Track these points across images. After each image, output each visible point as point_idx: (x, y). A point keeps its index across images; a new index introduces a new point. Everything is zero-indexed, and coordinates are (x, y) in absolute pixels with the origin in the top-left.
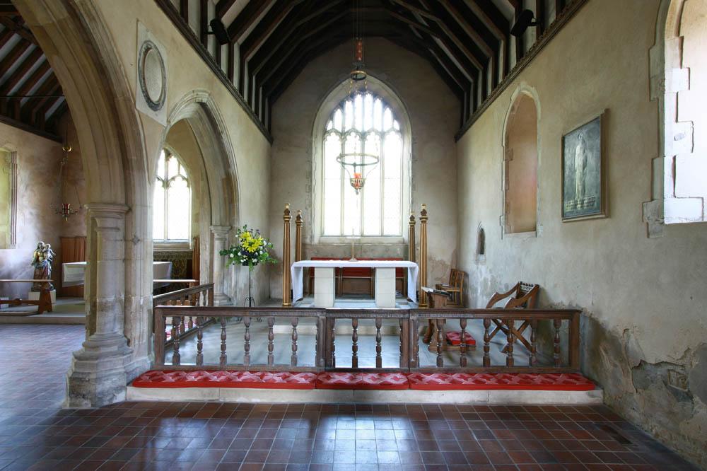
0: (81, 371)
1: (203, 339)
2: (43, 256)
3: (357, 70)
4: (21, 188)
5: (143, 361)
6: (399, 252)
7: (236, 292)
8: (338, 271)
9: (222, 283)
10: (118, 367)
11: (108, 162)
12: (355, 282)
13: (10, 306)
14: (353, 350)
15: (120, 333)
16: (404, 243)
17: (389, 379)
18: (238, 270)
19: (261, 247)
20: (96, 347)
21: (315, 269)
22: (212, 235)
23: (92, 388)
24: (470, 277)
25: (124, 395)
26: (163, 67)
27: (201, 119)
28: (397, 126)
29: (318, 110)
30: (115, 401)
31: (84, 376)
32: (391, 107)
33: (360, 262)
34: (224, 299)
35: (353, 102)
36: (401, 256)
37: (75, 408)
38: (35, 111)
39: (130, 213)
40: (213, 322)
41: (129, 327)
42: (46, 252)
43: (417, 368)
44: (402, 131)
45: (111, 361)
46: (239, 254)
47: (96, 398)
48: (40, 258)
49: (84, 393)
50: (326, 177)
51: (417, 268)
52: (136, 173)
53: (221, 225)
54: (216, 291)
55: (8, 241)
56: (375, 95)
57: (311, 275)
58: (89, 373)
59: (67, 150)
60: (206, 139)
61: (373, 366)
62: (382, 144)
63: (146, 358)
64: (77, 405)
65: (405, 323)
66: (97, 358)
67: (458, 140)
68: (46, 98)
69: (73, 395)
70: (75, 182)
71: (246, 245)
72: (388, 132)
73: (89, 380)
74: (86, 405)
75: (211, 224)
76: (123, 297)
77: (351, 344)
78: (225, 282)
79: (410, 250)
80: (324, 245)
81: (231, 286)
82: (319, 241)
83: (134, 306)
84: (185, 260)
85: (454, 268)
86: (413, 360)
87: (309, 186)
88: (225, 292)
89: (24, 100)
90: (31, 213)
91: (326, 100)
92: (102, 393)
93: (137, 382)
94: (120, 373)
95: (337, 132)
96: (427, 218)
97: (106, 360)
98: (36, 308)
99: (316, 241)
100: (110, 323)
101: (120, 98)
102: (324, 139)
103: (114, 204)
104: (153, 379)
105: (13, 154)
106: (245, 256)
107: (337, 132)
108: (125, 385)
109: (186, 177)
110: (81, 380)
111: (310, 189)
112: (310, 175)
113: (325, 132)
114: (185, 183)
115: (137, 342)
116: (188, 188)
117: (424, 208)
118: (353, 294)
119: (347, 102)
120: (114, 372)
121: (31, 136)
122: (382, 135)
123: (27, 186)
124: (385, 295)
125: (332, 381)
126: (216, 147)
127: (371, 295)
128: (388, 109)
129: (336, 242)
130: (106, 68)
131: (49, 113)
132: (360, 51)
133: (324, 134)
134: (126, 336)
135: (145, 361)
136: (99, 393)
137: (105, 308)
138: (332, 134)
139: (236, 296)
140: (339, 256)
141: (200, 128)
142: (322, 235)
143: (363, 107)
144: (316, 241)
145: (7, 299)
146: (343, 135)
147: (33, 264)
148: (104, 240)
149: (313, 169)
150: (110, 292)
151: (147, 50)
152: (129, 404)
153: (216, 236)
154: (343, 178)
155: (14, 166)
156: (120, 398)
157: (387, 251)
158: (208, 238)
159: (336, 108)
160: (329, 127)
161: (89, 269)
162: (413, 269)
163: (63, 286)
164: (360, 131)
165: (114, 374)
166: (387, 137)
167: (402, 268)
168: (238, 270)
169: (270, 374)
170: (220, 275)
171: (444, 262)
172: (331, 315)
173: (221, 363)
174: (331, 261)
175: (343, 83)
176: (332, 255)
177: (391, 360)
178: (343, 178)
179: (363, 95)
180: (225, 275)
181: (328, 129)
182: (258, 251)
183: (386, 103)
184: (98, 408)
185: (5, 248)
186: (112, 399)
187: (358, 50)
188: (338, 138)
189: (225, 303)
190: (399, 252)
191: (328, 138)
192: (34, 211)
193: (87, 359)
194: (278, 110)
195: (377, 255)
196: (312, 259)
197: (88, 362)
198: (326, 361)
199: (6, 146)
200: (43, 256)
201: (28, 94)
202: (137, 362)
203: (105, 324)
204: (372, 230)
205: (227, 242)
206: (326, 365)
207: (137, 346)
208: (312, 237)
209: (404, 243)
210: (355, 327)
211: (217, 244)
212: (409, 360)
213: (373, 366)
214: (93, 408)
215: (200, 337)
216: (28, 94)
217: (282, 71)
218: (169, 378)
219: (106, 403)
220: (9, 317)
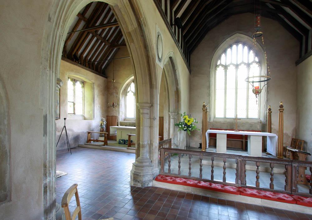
0: (137, 171)
1: (171, 163)
3: (257, 32)
4: (96, 96)
5: (156, 170)
6: (259, 127)
7: (179, 143)
8: (229, 136)
9: (174, 138)
10: (150, 172)
11: (146, 85)
12: (239, 142)
13: (94, 142)
14: (212, 172)
15: (148, 157)
16: (261, 123)
17: (227, 188)
18: (180, 133)
19: (193, 123)
20: (142, 162)
21: (217, 134)
22: (169, 116)
23: (141, 179)
24: (308, 144)
25: (152, 184)
26: (162, 43)
27: (169, 64)
28: (257, 59)
29: (213, 55)
30: (149, 186)
31: (138, 174)
32: (253, 50)
33: (240, 132)
34: (175, 146)
35: (231, 49)
36: (260, 130)
37: (135, 186)
38: (99, 66)
39: (152, 107)
40: (175, 154)
41: (152, 155)
42: (104, 121)
43: (297, 193)
44: (260, 63)
45: (147, 169)
46: (183, 126)
47: (143, 183)
48: (102, 124)
49: (139, 180)
50: (216, 88)
51: (277, 137)
52: (155, 90)
53: (174, 112)
54: (172, 142)
55: (92, 117)
56: (244, 44)
57: (246, 139)
58: (140, 173)
59: (113, 81)
60: (170, 73)
61: (268, 187)
62: (237, 71)
63: (157, 169)
64: (136, 185)
65: (289, 168)
66: (143, 167)
67: (298, 64)
68: (103, 61)
69: (135, 181)
70: (112, 94)
71: (186, 122)
72: (240, 64)
73: (140, 176)
74: (139, 185)
75: (169, 112)
76: (149, 142)
77: (223, 171)
78: (175, 138)
79: (266, 126)
80: (216, 122)
81: (177, 140)
82: (213, 120)
83: (154, 146)
85: (294, 137)
86: (294, 188)
87: (209, 93)
88: (175, 142)
89: (96, 63)
90: (99, 107)
91: (217, 50)
92: (145, 181)
93: (156, 179)
94: (150, 174)
95: (222, 66)
96: (283, 110)
97: (146, 168)
98: (103, 143)
99: (212, 120)
100: (145, 152)
101: (151, 58)
102: (216, 69)
103: (147, 103)
104: (161, 178)
105: (94, 83)
106: (186, 127)
107: (222, 66)
108: (152, 179)
110: (137, 175)
111: (209, 95)
112: (209, 87)
113: (217, 66)
114: (133, 94)
115: (155, 162)
117: (281, 104)
118: (232, 148)
119: (229, 49)
120: (148, 173)
121: (98, 76)
122: (248, 65)
123: (97, 96)
124: (255, 149)
125: (201, 185)
126: (173, 76)
127: (245, 149)
128: (252, 51)
129: (222, 121)
130: (148, 46)
131: (103, 67)
132: (259, 22)
133: (216, 67)
134: (150, 159)
135: (157, 170)
136: (144, 182)
137: (143, 146)
138: (230, 66)
139: (179, 145)
140: (224, 128)
141: (169, 68)
142: (215, 117)
144: (212, 120)
145: (93, 139)
146: (226, 67)
147: (100, 126)
148: (144, 118)
149: (211, 85)
150: (145, 140)
151: (159, 36)
152: (154, 189)
153: (171, 117)
154: (248, 89)
156: (150, 185)
157: (251, 127)
158: (167, 118)
159: (222, 53)
160: (218, 63)
161: (137, 130)
162: (271, 138)
163: (110, 135)
164: (236, 64)
165: (149, 174)
166: (240, 67)
167: (242, 135)
168: (180, 133)
169: (202, 182)
170: (173, 135)
171: (288, 134)
172: (244, 159)
173: (189, 175)
174: (223, 131)
175: (227, 40)
176: (221, 128)
177: (231, 180)
178: (248, 89)
179: (237, 45)
180: (175, 135)
181: (218, 64)
182: (192, 124)
183: (250, 48)
184: (144, 188)
185: (91, 120)
186: (148, 185)
187: (260, 22)
188: (223, 68)
189: (175, 147)
190: (259, 128)
191: (218, 69)
192: (99, 106)
193: (139, 167)
194: (192, 56)
195: (245, 129)
196: (210, 129)
197: (140, 168)
198: (241, 182)
199: (92, 81)
201: (97, 61)
202: (155, 170)
203: (144, 153)
204: (242, 115)
205: (176, 120)
206: (242, 184)
207: (155, 164)
208: (210, 118)
209: (261, 123)
210: (213, 161)
211: (172, 121)
212: (291, 188)
213: (268, 187)
214: (142, 187)
215: (170, 162)
216: (97, 61)
217: (197, 37)
218: (169, 179)
219: (146, 186)
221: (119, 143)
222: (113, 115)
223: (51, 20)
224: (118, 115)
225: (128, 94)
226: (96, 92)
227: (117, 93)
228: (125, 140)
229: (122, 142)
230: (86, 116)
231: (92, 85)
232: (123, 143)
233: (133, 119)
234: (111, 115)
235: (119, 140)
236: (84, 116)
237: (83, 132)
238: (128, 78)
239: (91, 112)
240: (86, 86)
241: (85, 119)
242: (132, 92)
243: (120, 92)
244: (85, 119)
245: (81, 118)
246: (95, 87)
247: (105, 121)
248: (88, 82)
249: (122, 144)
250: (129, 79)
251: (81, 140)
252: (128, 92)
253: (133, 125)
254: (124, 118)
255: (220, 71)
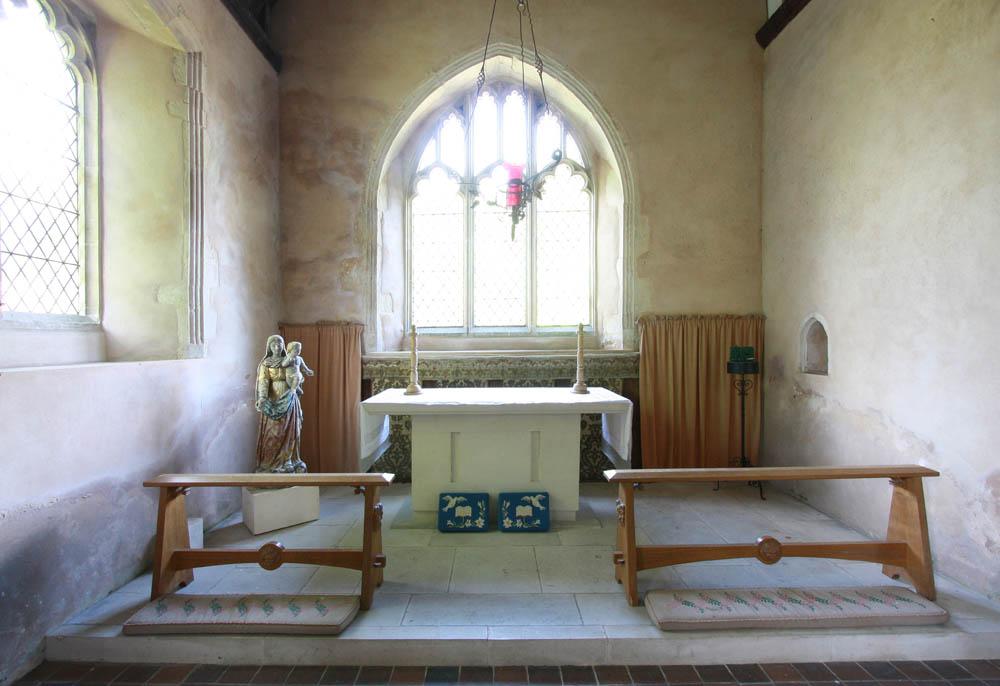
2: (283, 379)
4: (212, 169)
48: (278, 386)
55: (184, 335)
70: (314, 177)
84: (618, 379)
90: (231, 254)
105: (194, 57)
109: (580, 162)
116: (585, 195)
143: (532, 146)
155: (195, 101)
185: (176, 357)
192: (235, 247)
199: (181, 23)
200: (283, 379)
220: (275, 640)
221: (444, 529)
222: (333, 318)
223: (263, 566)
224: (362, 317)
225: (421, 186)
226: (217, 137)
227: (359, 174)
228: (485, 497)
229: (467, 511)
230: (123, 321)
231: (182, 68)
232: (480, 523)
233: (459, 335)
234: (315, 317)
235: (443, 503)
236: (100, 328)
237: (102, 488)
238: (441, 73)
239: (172, 295)
240: (120, 63)
241: (109, 352)
242: (451, 173)
243: (378, 167)
244: (109, 352)
245: (70, 346)
246: (211, 101)
247: (300, 360)
248: (141, 38)
249: (474, 530)
250: (441, 82)
251: (75, 574)
252: (425, 173)
253: (480, 372)
254: (400, 335)
255: (435, 194)
